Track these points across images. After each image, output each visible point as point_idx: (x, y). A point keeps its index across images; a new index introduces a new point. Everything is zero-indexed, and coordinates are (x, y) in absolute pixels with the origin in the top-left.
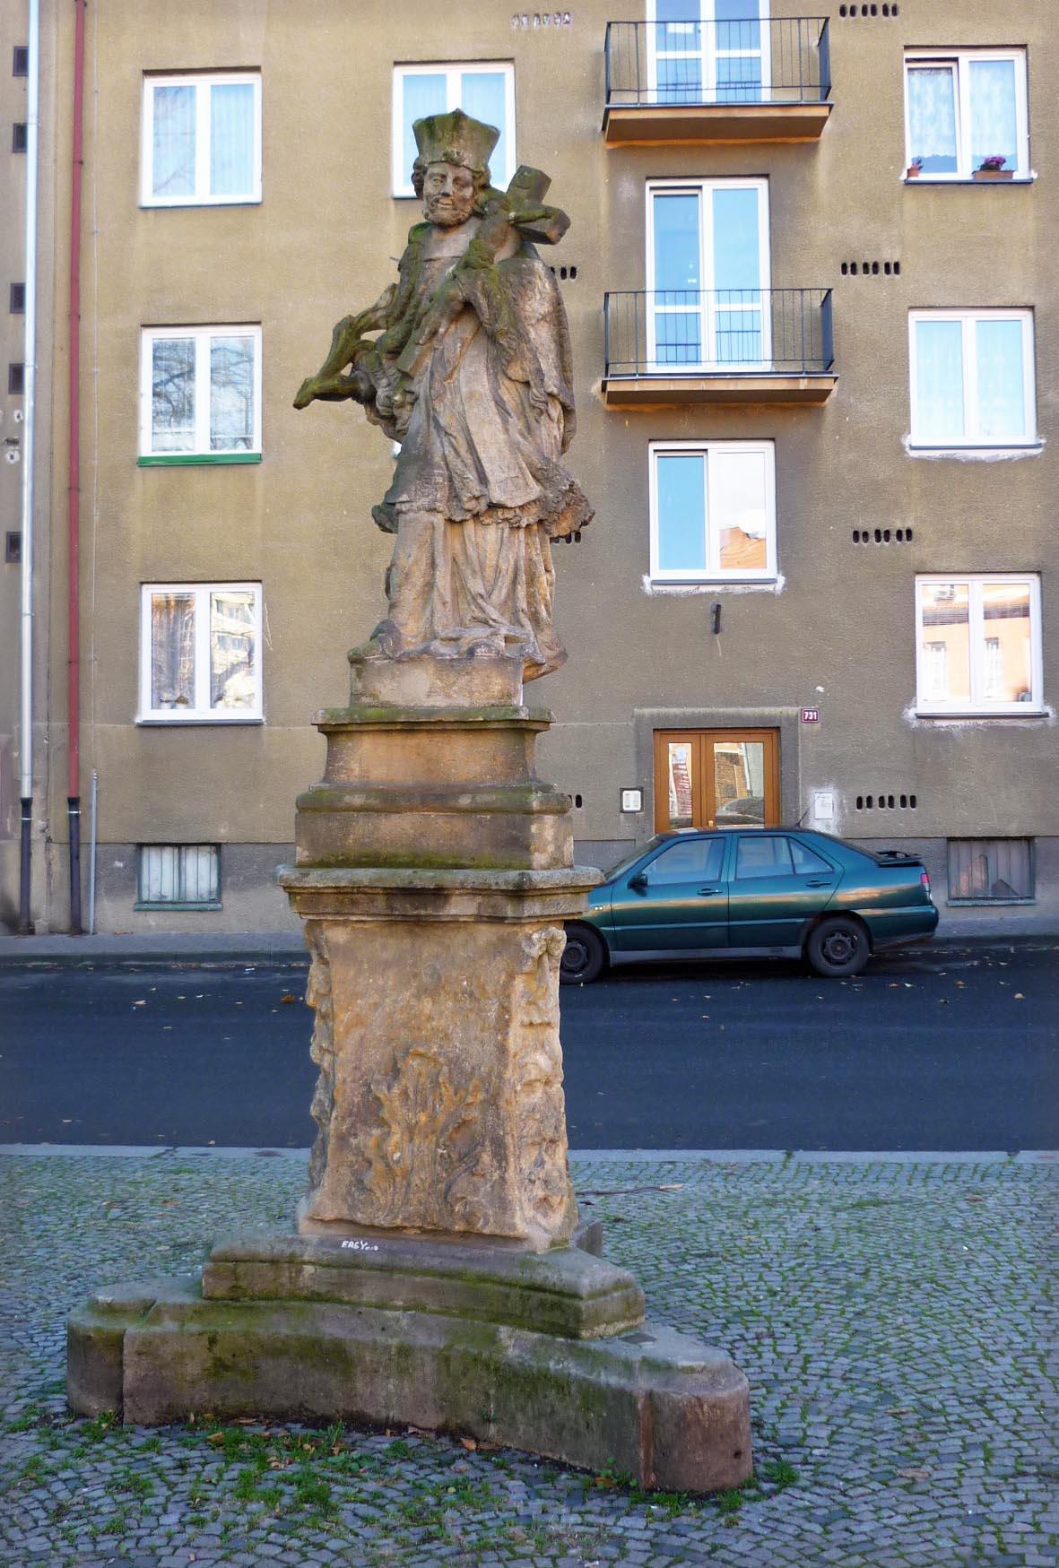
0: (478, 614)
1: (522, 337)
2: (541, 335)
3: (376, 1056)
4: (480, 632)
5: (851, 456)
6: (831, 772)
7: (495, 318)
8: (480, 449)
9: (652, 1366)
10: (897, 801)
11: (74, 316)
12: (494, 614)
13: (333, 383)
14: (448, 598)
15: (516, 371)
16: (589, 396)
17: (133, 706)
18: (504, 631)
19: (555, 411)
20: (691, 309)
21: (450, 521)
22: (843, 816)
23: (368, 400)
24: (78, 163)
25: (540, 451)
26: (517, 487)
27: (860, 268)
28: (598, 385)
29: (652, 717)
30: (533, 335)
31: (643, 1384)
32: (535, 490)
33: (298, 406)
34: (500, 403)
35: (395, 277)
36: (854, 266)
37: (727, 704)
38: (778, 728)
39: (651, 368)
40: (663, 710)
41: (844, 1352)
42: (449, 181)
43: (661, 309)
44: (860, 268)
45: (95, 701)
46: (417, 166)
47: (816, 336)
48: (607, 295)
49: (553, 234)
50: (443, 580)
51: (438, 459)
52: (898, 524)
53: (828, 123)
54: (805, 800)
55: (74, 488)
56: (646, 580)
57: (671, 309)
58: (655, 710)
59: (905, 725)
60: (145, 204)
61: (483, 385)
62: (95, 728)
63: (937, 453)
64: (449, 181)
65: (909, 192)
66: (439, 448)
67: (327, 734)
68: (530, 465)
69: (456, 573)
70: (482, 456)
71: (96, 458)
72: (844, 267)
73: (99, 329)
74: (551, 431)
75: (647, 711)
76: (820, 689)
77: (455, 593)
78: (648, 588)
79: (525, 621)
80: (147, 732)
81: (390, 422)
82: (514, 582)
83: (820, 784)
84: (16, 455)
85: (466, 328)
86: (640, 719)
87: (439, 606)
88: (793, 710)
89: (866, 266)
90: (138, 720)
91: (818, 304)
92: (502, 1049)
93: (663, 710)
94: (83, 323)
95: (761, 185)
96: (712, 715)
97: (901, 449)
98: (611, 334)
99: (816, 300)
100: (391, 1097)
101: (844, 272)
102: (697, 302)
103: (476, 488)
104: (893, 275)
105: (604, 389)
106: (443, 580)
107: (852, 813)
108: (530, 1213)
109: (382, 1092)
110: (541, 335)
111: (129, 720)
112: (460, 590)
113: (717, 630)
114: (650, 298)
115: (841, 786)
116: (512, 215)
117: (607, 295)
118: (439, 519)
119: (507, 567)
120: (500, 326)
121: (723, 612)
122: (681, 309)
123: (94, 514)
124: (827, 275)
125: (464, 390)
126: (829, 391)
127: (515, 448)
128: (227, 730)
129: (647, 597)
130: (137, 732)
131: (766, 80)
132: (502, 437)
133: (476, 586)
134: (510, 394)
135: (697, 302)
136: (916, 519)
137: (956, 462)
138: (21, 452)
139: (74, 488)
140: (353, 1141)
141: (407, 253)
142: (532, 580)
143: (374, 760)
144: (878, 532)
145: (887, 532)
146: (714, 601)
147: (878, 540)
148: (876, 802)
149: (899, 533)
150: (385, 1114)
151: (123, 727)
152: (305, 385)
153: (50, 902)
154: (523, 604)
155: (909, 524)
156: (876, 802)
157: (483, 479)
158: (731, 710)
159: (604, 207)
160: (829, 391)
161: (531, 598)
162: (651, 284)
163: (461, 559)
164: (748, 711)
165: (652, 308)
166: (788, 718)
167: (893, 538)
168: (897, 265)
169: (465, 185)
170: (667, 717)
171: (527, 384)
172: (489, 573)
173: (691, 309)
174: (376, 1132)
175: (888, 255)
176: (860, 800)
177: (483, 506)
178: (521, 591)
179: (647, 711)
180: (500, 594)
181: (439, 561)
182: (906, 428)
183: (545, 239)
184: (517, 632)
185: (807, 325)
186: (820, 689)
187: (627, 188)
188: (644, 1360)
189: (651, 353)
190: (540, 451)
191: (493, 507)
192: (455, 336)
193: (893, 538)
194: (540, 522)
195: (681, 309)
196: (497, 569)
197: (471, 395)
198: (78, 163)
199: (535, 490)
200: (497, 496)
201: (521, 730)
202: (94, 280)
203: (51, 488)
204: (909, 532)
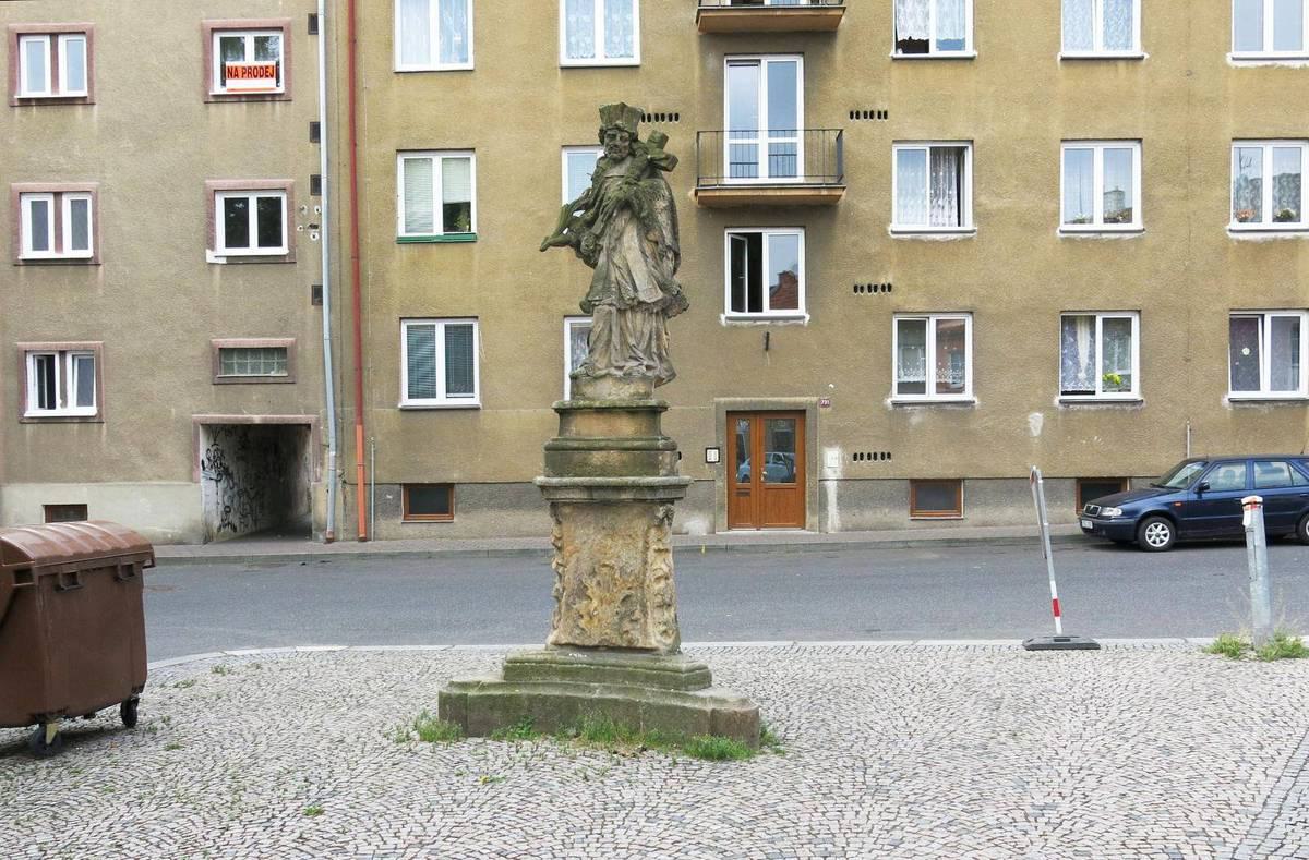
0: (632, 354)
1: (655, 220)
2: (663, 218)
3: (585, 567)
4: (633, 363)
5: (853, 238)
6: (838, 437)
7: (641, 209)
8: (634, 275)
9: (715, 700)
10: (879, 456)
11: (354, 144)
12: (641, 355)
13: (560, 238)
14: (618, 347)
15: (651, 236)
16: (686, 198)
17: (398, 397)
18: (645, 363)
19: (670, 255)
20: (752, 141)
21: (619, 310)
22: (845, 464)
23: (576, 246)
24: (353, 42)
25: (663, 275)
26: (652, 293)
27: (862, 115)
28: (692, 192)
29: (725, 404)
30: (659, 218)
31: (709, 708)
32: (660, 295)
33: (542, 250)
34: (643, 252)
35: (590, 184)
36: (858, 113)
37: (773, 395)
38: (804, 411)
39: (727, 181)
40: (732, 399)
41: (809, 710)
42: (618, 138)
43: (734, 141)
44: (862, 115)
45: (374, 394)
46: (601, 130)
47: (836, 162)
48: (698, 133)
49: (670, 166)
50: (615, 339)
51: (613, 279)
52: (883, 281)
53: (843, 20)
54: (821, 455)
55: (356, 257)
56: (723, 317)
57: (739, 141)
58: (727, 399)
59: (885, 408)
60: (397, 70)
61: (635, 243)
62: (374, 411)
63: (909, 236)
64: (618, 138)
65: (895, 65)
66: (614, 274)
67: (561, 414)
68: (658, 283)
69: (622, 333)
70: (635, 278)
71: (369, 238)
72: (852, 114)
73: (370, 152)
74: (669, 264)
75: (723, 399)
76: (831, 385)
77: (621, 345)
78: (723, 321)
79: (656, 358)
80: (406, 414)
81: (590, 259)
82: (650, 338)
83: (831, 446)
84: (317, 236)
85: (626, 215)
86: (718, 404)
87: (614, 351)
88: (814, 399)
89: (865, 113)
90: (400, 406)
91: (834, 139)
92: (645, 562)
93: (732, 399)
94: (358, 148)
95: (800, 61)
96: (763, 402)
97: (886, 232)
98: (702, 158)
99: (833, 136)
100: (591, 583)
101: (852, 117)
102: (756, 137)
103: (632, 294)
104: (883, 120)
105: (696, 194)
106: (615, 339)
107: (851, 464)
108: (659, 637)
109: (588, 582)
110: (663, 218)
111: (395, 406)
112: (624, 342)
113: (767, 349)
114: (726, 134)
115: (844, 446)
116: (649, 157)
117: (698, 133)
118: (613, 309)
119: (647, 332)
120: (643, 214)
121: (771, 337)
122: (746, 141)
123: (369, 273)
124: (839, 119)
125: (626, 245)
126: (840, 196)
127: (651, 274)
128: (431, 414)
129: (723, 328)
130: (400, 413)
131: (764, 124)
132: (644, 269)
133: (632, 341)
134: (648, 249)
135: (756, 137)
136: (894, 278)
137: (921, 241)
138: (320, 233)
139: (356, 257)
140: (574, 607)
141: (596, 172)
142: (659, 338)
143: (588, 428)
144: (869, 287)
145: (876, 287)
146: (766, 330)
147: (870, 291)
148: (866, 457)
149: (883, 288)
150: (589, 592)
151: (392, 410)
152: (547, 238)
153: (345, 521)
154: (654, 350)
155: (890, 280)
156: (866, 457)
157: (635, 289)
158: (776, 399)
159: (697, 74)
160: (840, 196)
161: (659, 347)
162: (727, 127)
163: (625, 328)
164: (785, 399)
165: (728, 140)
166: (811, 404)
167: (880, 290)
168: (886, 113)
169: (626, 140)
170: (735, 403)
171: (657, 243)
172: (638, 334)
173: (752, 141)
174: (585, 602)
175: (880, 106)
176: (855, 455)
177: (635, 303)
178: (654, 344)
179: (723, 399)
180: (643, 345)
181: (614, 328)
182: (890, 221)
183: (666, 169)
184: (652, 363)
185: (827, 152)
186: (831, 385)
187: (712, 62)
188: (712, 697)
189: (727, 172)
190: (663, 275)
191: (641, 303)
192: (621, 221)
193: (880, 290)
194: (663, 310)
195: (746, 141)
196: (642, 333)
197: (630, 248)
198: (353, 42)
199: (660, 295)
200: (642, 297)
201: (655, 412)
202: (365, 120)
203: (340, 257)
204: (890, 287)
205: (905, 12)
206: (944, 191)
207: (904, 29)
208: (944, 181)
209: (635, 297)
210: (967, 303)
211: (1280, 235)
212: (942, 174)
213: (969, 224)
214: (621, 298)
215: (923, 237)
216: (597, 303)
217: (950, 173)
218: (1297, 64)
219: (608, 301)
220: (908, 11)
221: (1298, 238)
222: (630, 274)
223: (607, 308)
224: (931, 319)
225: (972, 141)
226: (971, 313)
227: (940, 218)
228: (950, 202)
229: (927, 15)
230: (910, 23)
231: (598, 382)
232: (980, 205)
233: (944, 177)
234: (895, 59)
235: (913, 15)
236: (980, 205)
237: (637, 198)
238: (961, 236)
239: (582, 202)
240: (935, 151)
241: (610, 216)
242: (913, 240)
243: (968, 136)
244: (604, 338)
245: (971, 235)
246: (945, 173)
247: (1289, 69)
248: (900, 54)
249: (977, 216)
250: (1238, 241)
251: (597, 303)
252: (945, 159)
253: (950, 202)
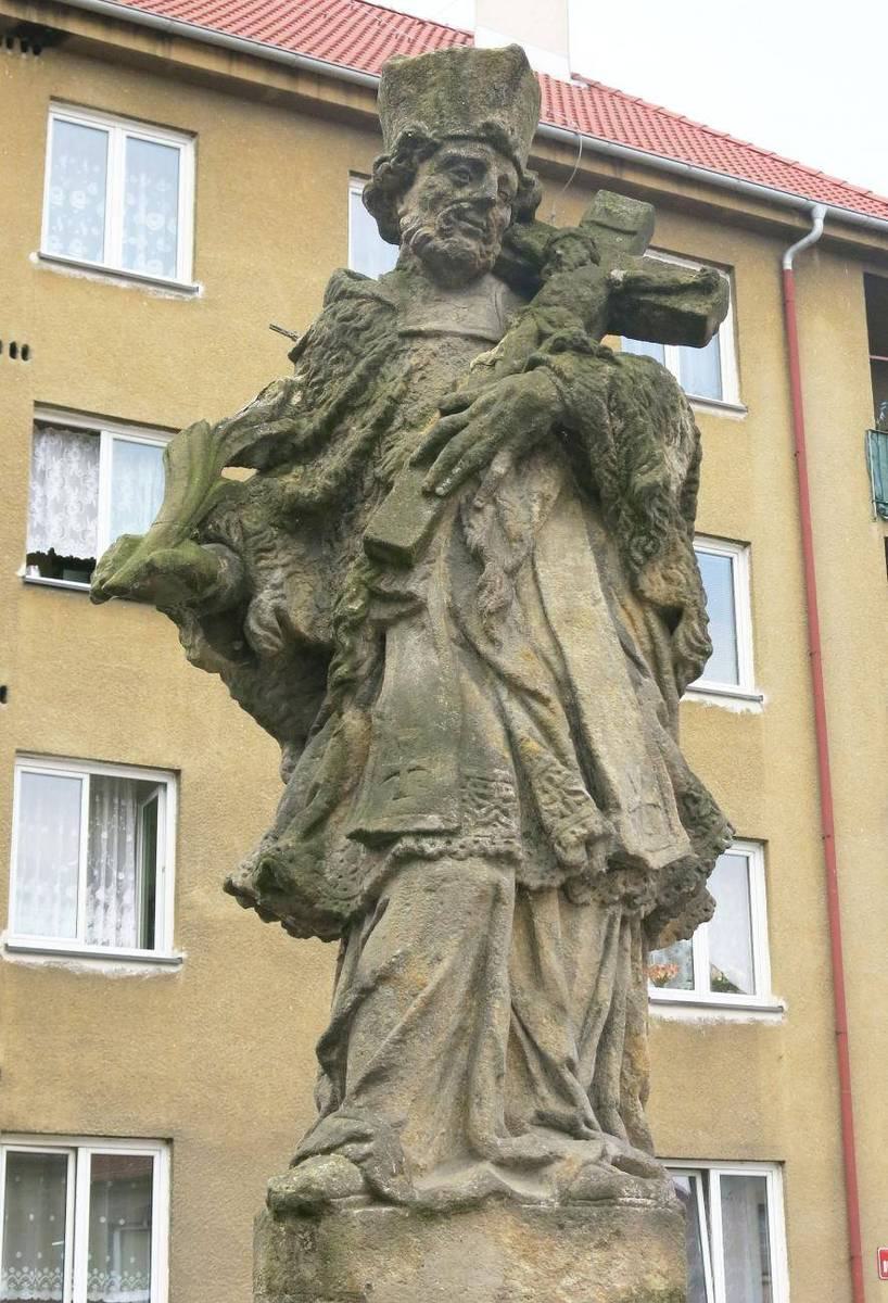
63: (41, 961)
65: (29, 594)
137: (66, 974)
157: (603, 798)
205: (45, 497)
206: (108, 871)
207: (42, 530)
208: (109, 850)
209: (606, 837)
210: (160, 1118)
211: (729, 1016)
212: (105, 835)
213: (165, 946)
214: (538, 832)
215: (72, 964)
216: (429, 846)
217: (122, 834)
218: (738, 707)
219: (479, 837)
220: (51, 497)
221: (758, 1023)
222: (579, 734)
223: (484, 873)
224: (81, 1152)
225: (177, 773)
226: (169, 1141)
227: (99, 927)
228: (119, 897)
229: (92, 512)
230: (54, 522)
231: (439, 1233)
232: (191, 908)
233: (110, 840)
234: (29, 584)
235: (60, 507)
236: (191, 908)
237: (619, 410)
238: (150, 969)
239: (264, 430)
240: (96, 781)
241: (473, 475)
242: (51, 971)
243: (168, 760)
244: (449, 1016)
245: (172, 970)
246: (111, 835)
247: (725, 712)
248: (34, 574)
249: (182, 929)
250: (662, 1022)
251: (429, 846)
252: (112, 804)
253: (119, 897)
